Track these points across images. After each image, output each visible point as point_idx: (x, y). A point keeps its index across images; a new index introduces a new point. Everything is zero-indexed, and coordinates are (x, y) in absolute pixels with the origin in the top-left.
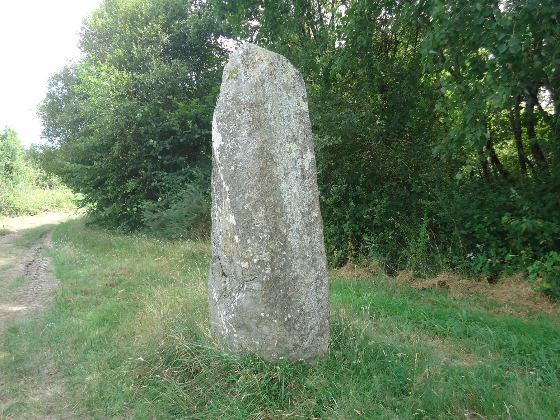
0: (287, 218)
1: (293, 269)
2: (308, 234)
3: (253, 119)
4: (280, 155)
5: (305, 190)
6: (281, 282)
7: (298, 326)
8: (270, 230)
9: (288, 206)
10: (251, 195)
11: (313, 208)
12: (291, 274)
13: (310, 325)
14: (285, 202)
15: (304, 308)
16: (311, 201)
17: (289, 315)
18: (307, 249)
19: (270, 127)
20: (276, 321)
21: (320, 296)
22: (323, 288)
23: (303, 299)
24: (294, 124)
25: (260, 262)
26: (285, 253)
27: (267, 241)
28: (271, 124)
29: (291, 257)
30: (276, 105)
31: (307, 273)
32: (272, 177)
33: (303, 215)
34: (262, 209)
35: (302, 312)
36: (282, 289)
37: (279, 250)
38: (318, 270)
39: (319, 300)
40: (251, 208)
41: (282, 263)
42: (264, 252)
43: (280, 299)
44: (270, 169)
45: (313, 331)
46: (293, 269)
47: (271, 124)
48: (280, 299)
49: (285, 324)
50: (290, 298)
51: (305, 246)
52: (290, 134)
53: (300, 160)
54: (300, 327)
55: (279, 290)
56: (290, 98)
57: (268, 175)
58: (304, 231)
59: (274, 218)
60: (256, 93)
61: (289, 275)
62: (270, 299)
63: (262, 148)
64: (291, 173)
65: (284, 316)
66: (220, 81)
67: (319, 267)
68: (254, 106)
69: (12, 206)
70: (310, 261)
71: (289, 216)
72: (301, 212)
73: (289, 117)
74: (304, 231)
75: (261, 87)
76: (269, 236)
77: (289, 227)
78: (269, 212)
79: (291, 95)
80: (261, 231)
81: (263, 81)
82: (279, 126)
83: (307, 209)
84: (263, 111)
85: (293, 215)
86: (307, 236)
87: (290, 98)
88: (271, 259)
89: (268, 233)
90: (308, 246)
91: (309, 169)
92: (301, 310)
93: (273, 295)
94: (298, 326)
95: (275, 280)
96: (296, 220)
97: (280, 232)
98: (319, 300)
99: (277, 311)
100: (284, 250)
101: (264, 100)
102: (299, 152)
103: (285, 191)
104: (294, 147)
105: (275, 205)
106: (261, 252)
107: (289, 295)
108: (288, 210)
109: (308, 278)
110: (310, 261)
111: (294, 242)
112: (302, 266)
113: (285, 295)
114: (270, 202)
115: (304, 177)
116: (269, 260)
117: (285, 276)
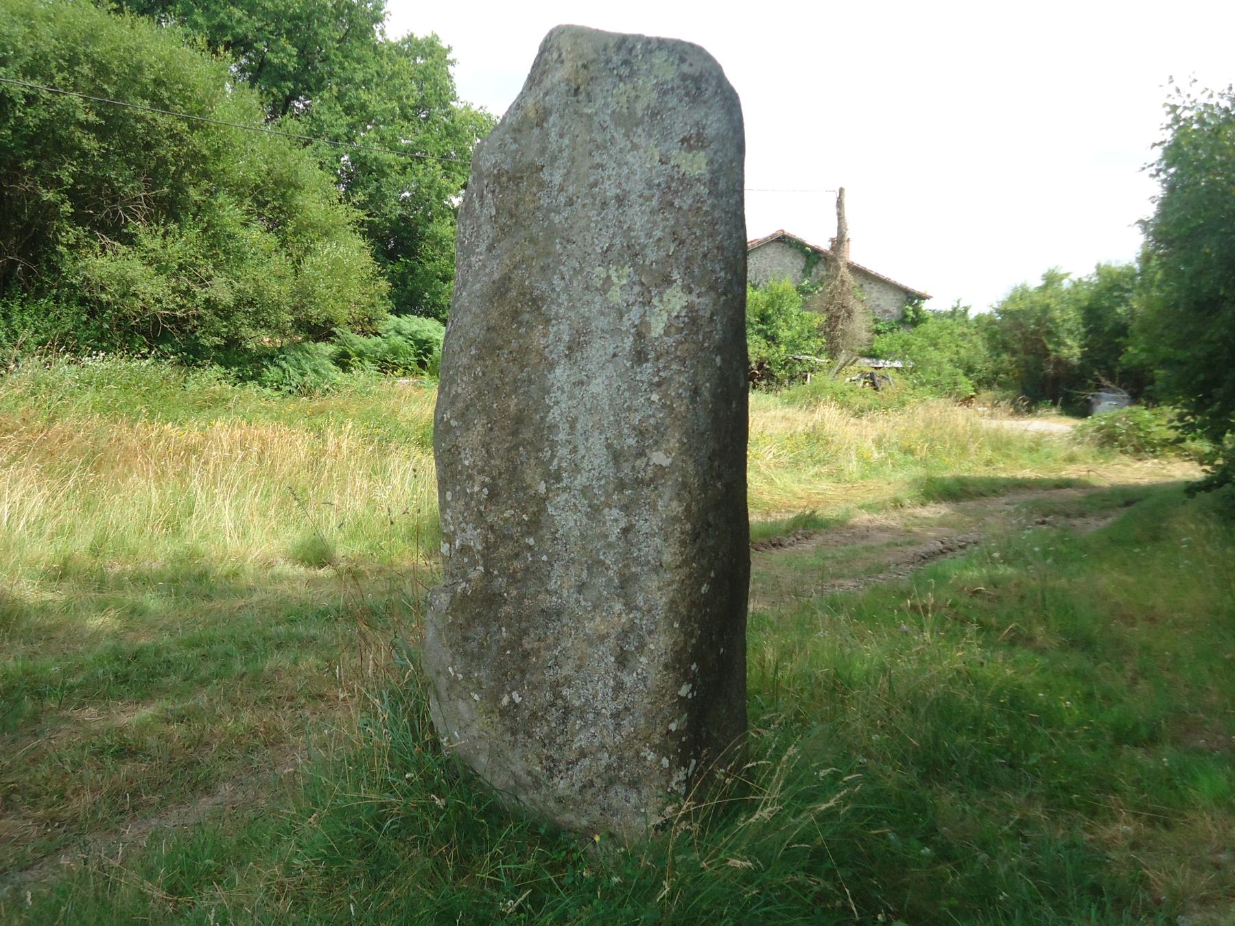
0: (553, 456)
1: (552, 585)
2: (626, 508)
3: (497, 210)
4: (564, 297)
5: (634, 390)
6: (508, 609)
7: (540, 731)
8: (493, 478)
9: (564, 427)
10: (460, 390)
11: (656, 443)
12: (540, 597)
13: (580, 741)
14: (554, 415)
15: (566, 692)
16: (652, 421)
17: (515, 695)
18: (610, 545)
19: (551, 232)
20: (476, 697)
21: (628, 680)
22: (643, 660)
23: (568, 670)
24: (637, 217)
25: (465, 550)
26: (531, 541)
27: (480, 503)
28: (557, 219)
29: (550, 556)
30: (584, 169)
31: (595, 607)
32: (524, 351)
33: (617, 457)
34: (479, 425)
35: (560, 702)
36: (508, 626)
37: (516, 531)
38: (637, 608)
39: (619, 687)
40: (456, 419)
41: (517, 564)
42: (471, 526)
43: (494, 648)
44: (522, 330)
45: (586, 762)
46: (552, 585)
47: (557, 219)
48: (494, 648)
49: (503, 713)
50: (526, 655)
51: (606, 536)
52: (617, 241)
53: (636, 312)
54: (547, 736)
55: (500, 627)
56: (635, 147)
57: (514, 345)
58: (608, 496)
59: (508, 450)
60: (514, 147)
61: (534, 597)
62: (466, 639)
63: (506, 278)
64: (598, 343)
65: (502, 691)
66: (1135, 399)
67: (640, 601)
68: (504, 179)
69: (1142, 434)
70: (611, 580)
71: (562, 452)
72: (609, 446)
73: (620, 200)
74: (608, 496)
75: (536, 131)
76: (486, 491)
77: (558, 479)
78: (496, 433)
79: (641, 140)
80: (470, 477)
81: (544, 115)
82: (583, 223)
83: (631, 441)
84: (534, 189)
85: (575, 450)
86: (615, 512)
87: (635, 147)
88: (487, 548)
89: (483, 485)
90: (612, 539)
91: (667, 333)
92: (558, 695)
93: (478, 631)
94: (540, 731)
95: (491, 600)
96: (585, 464)
97: (524, 489)
98: (619, 687)
99: (481, 674)
100: (529, 534)
101: (539, 161)
102: (637, 289)
103: (561, 389)
104: (621, 276)
105: (519, 420)
106: (463, 525)
107: (527, 647)
108: (562, 436)
109: (598, 619)
110: (611, 580)
111: (566, 516)
112: (581, 588)
113: (515, 643)
114: (503, 411)
115: (640, 356)
116: (480, 548)
117: (522, 597)
